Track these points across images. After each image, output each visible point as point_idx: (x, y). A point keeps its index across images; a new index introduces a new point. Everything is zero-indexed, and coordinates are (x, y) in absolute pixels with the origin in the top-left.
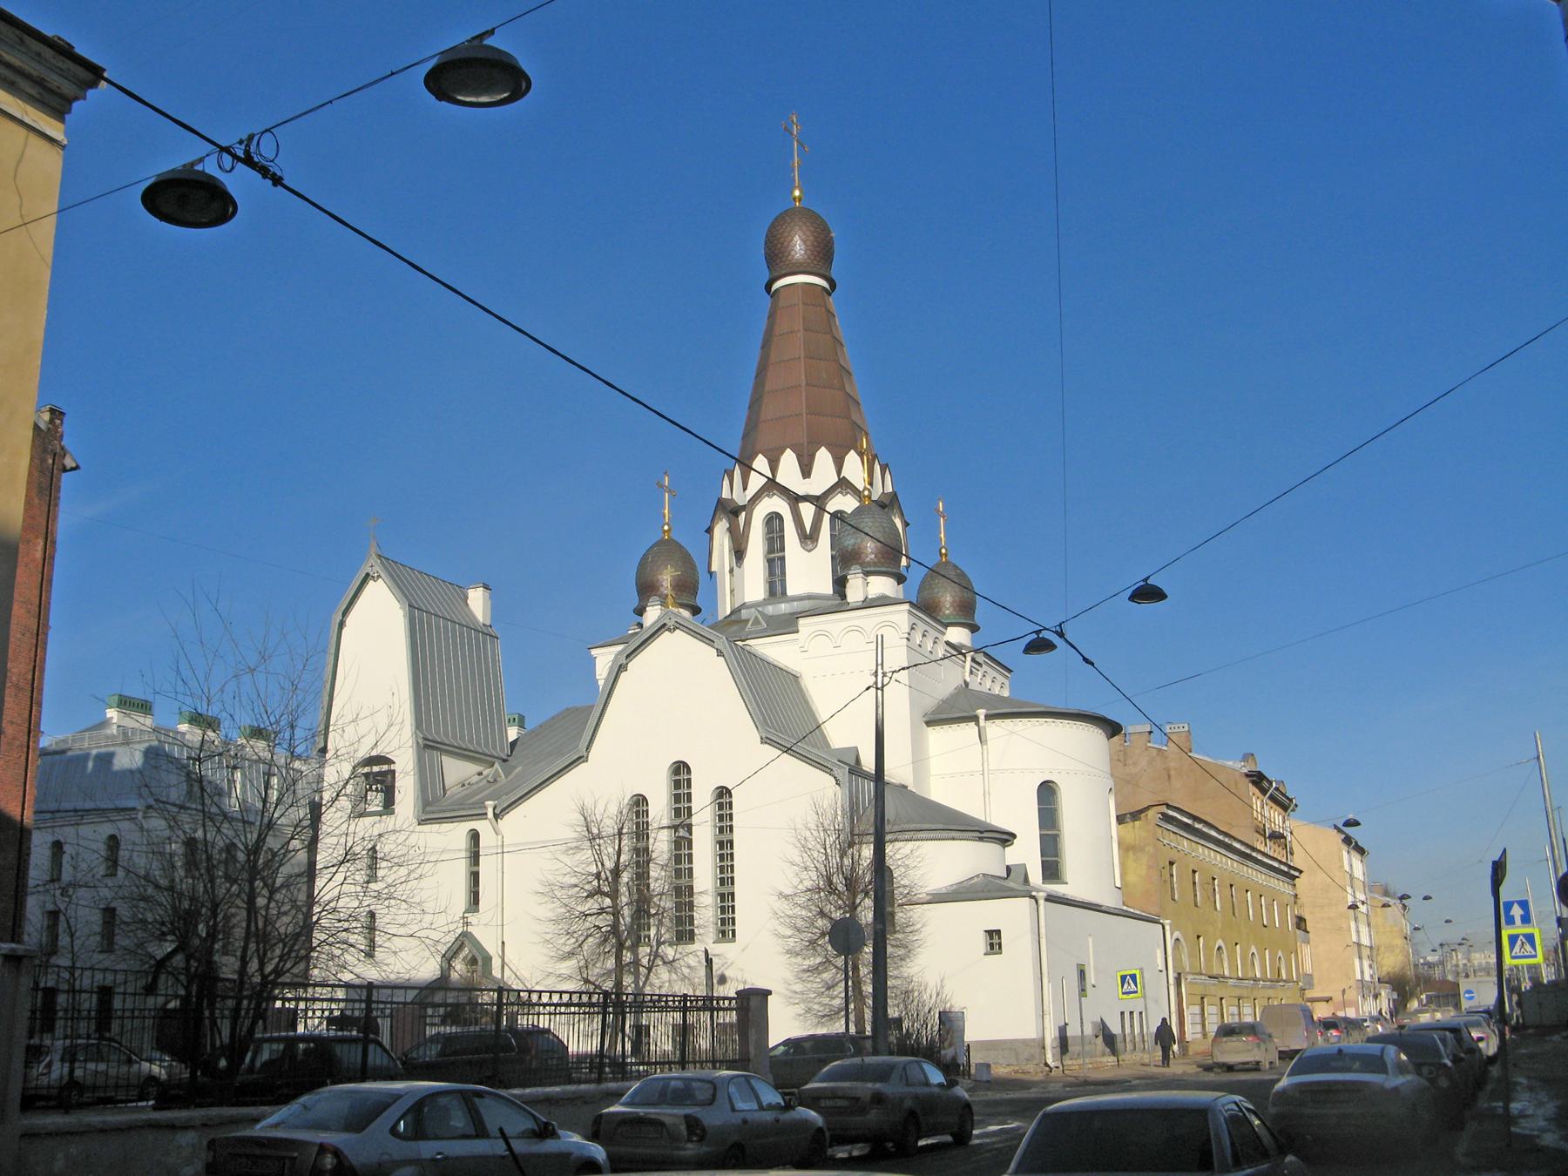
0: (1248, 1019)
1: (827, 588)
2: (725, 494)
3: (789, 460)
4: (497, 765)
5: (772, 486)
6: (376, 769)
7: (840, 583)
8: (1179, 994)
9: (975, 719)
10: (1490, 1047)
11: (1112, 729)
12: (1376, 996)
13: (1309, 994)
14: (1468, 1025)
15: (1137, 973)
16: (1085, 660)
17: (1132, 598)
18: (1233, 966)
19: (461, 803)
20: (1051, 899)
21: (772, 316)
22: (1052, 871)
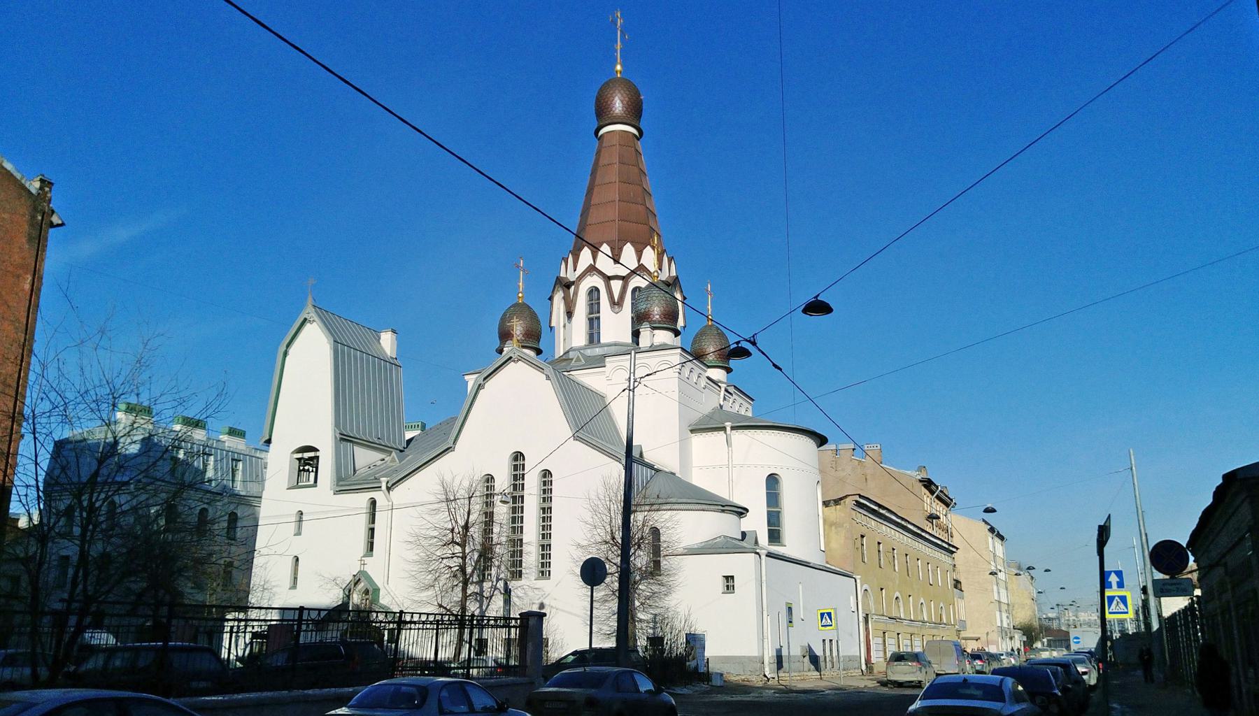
0: (918, 650)
1: (628, 339)
2: (562, 274)
4: (394, 454)
5: (592, 269)
6: (307, 455)
7: (636, 334)
8: (867, 629)
9: (724, 429)
10: (1092, 679)
11: (821, 440)
12: (1011, 638)
13: (963, 634)
14: (1076, 661)
16: (775, 365)
17: (805, 311)
18: (907, 611)
19: (365, 481)
20: (769, 555)
21: (598, 153)
22: (775, 536)
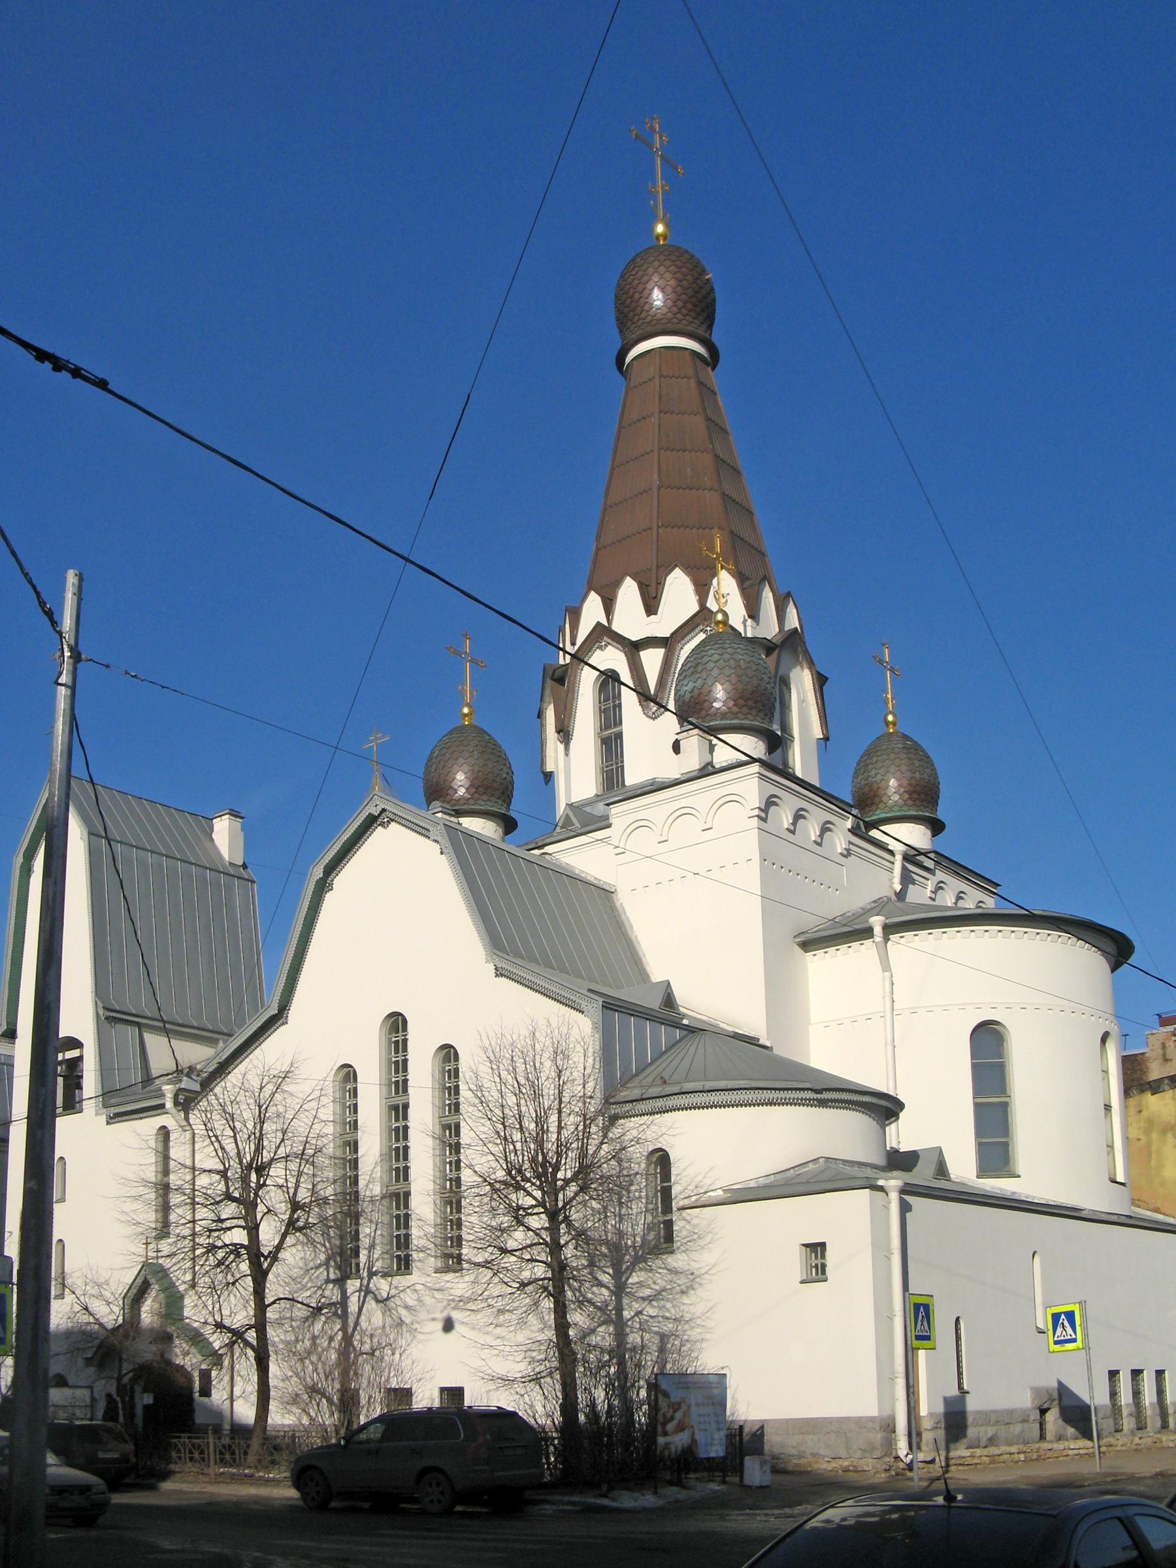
3: (629, 592)
5: (603, 634)
11: (1118, 949)
15: (1076, 1309)
22: (995, 1150)
